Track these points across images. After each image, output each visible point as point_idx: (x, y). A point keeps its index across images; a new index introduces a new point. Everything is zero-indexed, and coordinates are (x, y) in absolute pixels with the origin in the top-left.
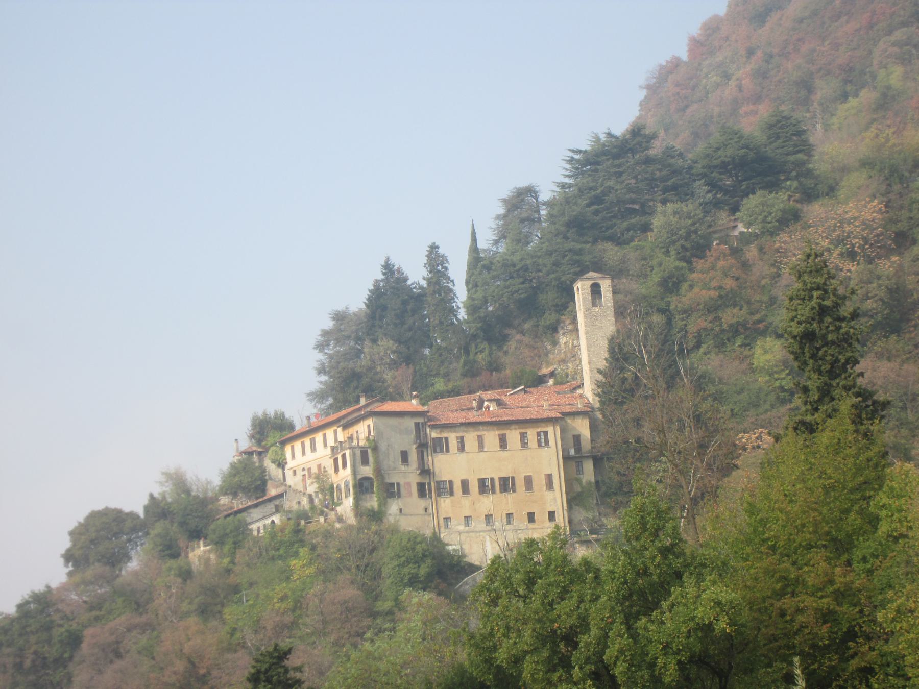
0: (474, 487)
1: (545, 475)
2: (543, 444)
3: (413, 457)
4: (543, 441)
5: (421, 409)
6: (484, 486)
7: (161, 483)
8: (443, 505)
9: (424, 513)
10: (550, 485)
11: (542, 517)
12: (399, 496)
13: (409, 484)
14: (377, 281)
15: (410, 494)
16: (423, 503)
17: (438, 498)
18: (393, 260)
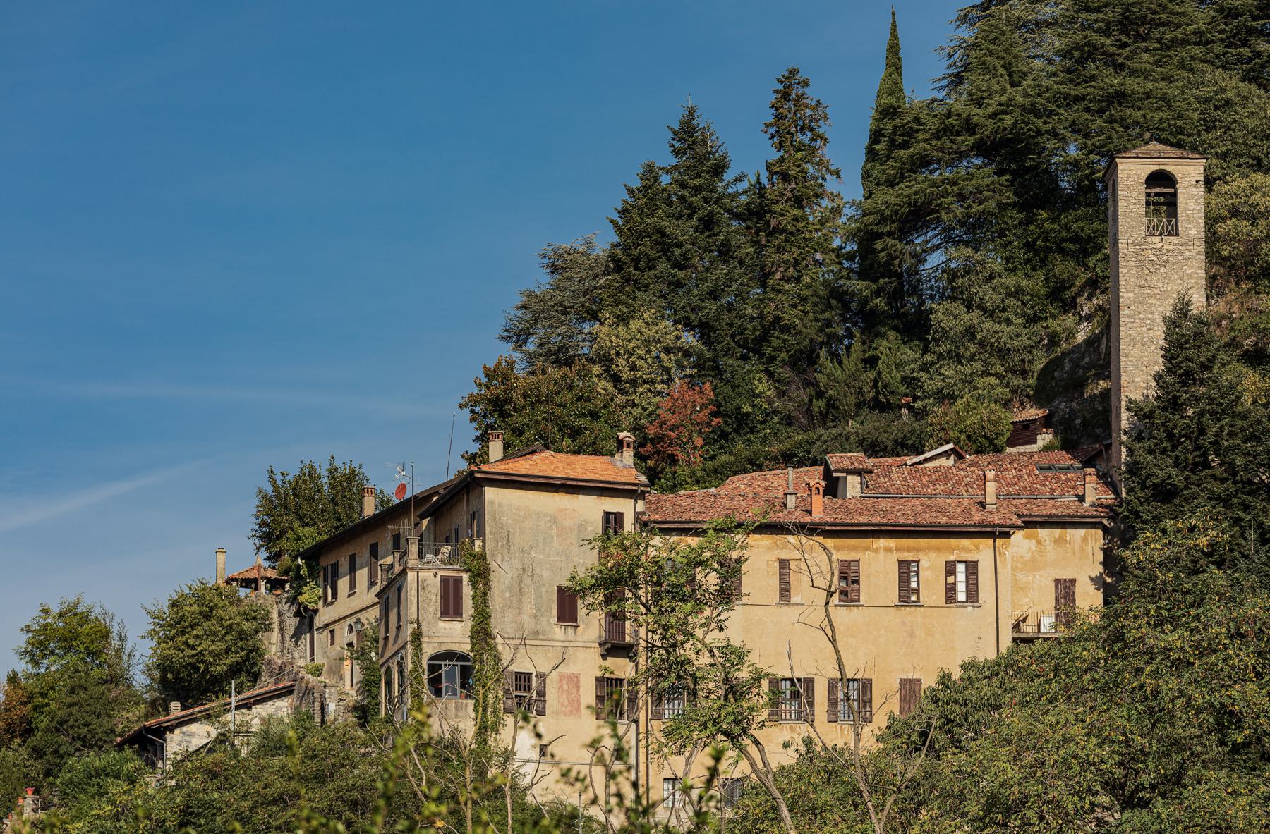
2: (962, 597)
4: (961, 587)
13: (574, 680)
18: (701, 121)
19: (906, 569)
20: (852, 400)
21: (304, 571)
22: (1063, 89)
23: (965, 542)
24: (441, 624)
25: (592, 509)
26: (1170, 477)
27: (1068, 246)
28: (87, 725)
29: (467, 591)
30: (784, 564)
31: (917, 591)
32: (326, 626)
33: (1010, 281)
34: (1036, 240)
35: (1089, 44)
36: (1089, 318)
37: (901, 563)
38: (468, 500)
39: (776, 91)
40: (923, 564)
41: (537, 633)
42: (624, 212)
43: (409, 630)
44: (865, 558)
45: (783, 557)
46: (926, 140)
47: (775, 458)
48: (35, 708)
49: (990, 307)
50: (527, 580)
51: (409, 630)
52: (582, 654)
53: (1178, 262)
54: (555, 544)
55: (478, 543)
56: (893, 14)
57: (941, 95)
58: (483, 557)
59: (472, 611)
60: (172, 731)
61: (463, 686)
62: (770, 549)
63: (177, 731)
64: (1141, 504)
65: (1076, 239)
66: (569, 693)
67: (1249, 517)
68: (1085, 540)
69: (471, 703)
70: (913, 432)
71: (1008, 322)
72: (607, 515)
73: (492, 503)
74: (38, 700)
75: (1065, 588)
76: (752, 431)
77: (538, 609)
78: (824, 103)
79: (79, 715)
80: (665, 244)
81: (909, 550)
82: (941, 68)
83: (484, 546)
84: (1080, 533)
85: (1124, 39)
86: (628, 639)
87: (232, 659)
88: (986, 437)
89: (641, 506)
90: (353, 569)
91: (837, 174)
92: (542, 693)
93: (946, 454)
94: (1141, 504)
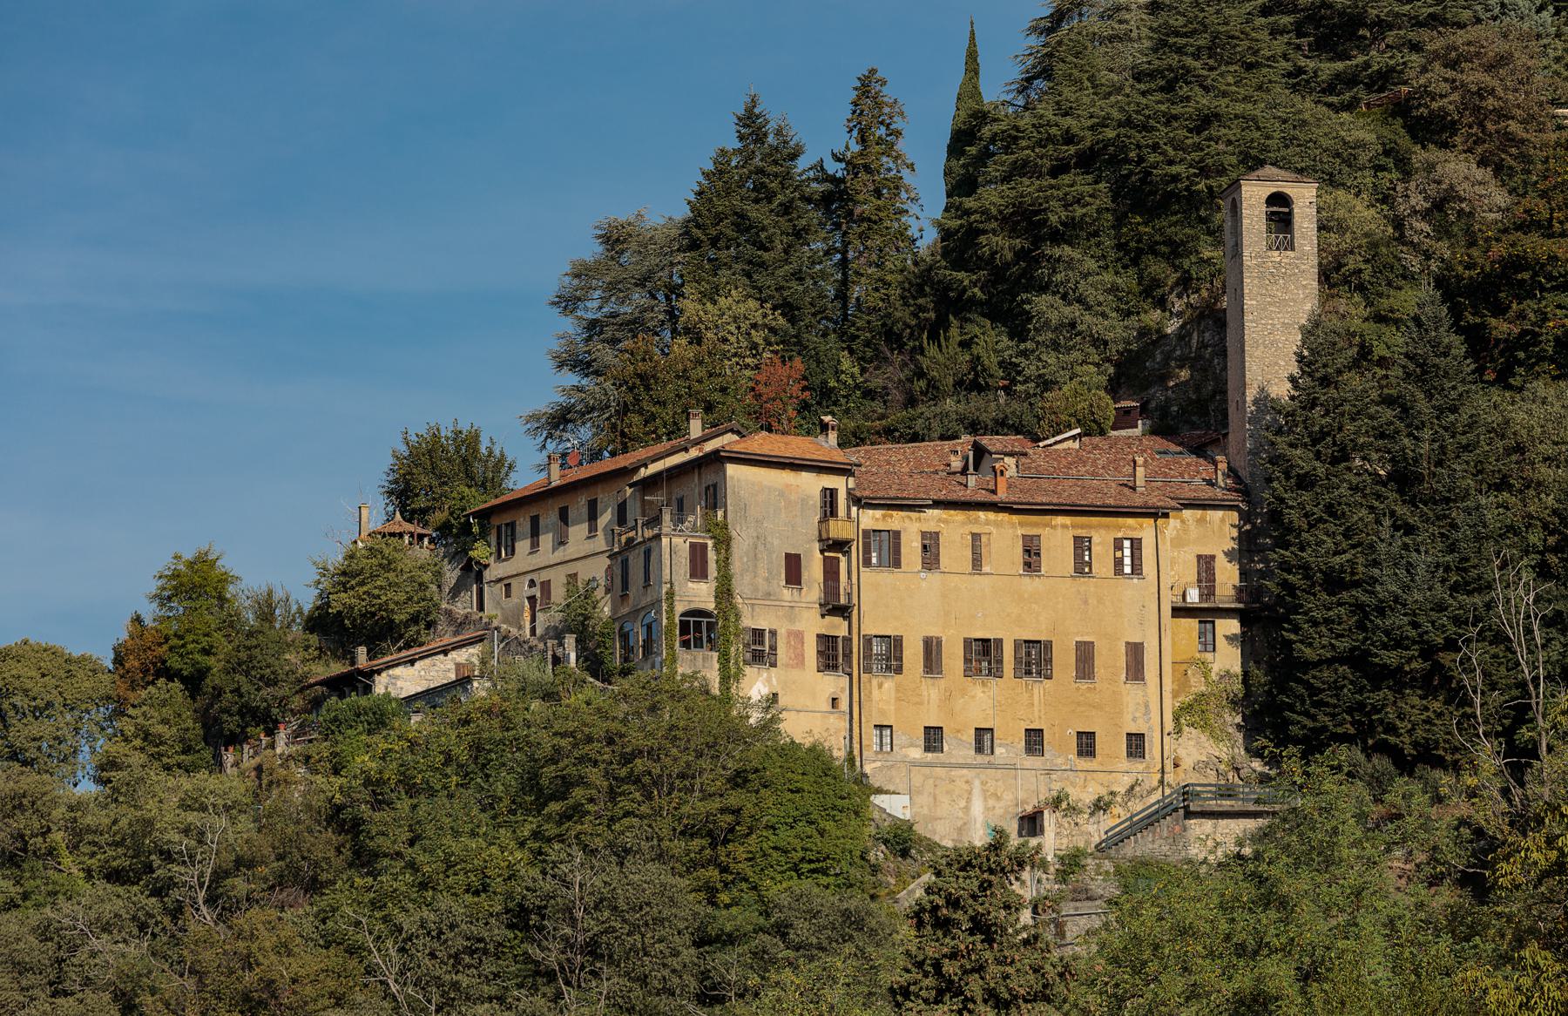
0: (953, 657)
1: (1128, 643)
2: (1127, 570)
3: (814, 569)
4: (1127, 561)
5: (839, 456)
6: (983, 654)
7: (206, 554)
8: (875, 693)
9: (829, 708)
10: (1135, 670)
11: (1111, 745)
12: (773, 665)
13: (799, 636)
14: (723, 152)
15: (800, 661)
16: (834, 684)
17: (864, 677)
18: (774, 113)
20: (951, 380)
21: (476, 529)
22: (1163, 108)
23: (1130, 521)
24: (690, 584)
25: (812, 485)
26: (1315, 469)
27: (1164, 249)
28: (268, 666)
29: (712, 555)
30: (976, 537)
31: (1090, 564)
32: (500, 580)
33: (1108, 277)
34: (1128, 242)
35: (1183, 67)
36: (1180, 314)
38: (700, 474)
39: (856, 89)
40: (1095, 540)
41: (770, 594)
42: (700, 193)
43: (665, 588)
44: (1045, 533)
45: (1206, 551)
46: (1027, 148)
47: (878, 433)
48: (171, 649)
49: (1091, 302)
50: (761, 548)
51: (665, 588)
52: (806, 614)
53: (1295, 274)
54: (783, 515)
55: (720, 513)
56: (972, 23)
58: (725, 526)
59: (716, 574)
60: (379, 674)
61: (710, 640)
62: (964, 523)
63: (384, 674)
64: (1286, 491)
65: (1169, 242)
66: (795, 648)
67: (1382, 506)
68: (1223, 520)
69: (715, 655)
70: (1013, 413)
71: (1104, 315)
73: (732, 478)
74: (174, 642)
75: (1206, 564)
76: (835, 403)
77: (770, 573)
78: (900, 101)
79: (260, 657)
80: (743, 223)
81: (1082, 527)
82: (1016, 73)
83: (725, 517)
84: (1219, 514)
85: (1211, 62)
86: (843, 601)
87: (412, 609)
88: (1094, 421)
89: (851, 482)
90: (535, 533)
91: (911, 167)
92: (773, 648)
93: (1074, 438)
94: (1286, 491)
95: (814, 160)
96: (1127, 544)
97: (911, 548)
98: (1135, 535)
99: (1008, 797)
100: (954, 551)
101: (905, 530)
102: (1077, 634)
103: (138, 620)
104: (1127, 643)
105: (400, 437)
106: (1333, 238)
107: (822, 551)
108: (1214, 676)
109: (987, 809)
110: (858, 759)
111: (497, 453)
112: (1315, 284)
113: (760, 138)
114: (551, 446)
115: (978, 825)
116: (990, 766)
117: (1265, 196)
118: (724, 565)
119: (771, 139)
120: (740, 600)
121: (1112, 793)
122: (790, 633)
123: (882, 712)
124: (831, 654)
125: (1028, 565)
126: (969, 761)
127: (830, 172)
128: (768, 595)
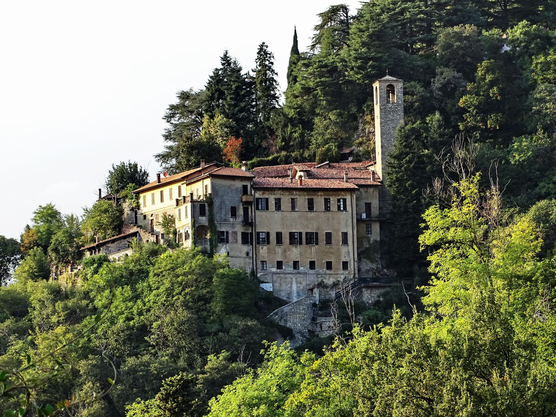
0: (286, 239)
2: (342, 209)
3: (241, 212)
4: (342, 206)
6: (295, 239)
8: (261, 251)
9: (246, 256)
12: (227, 242)
14: (216, 69)
16: (246, 248)
17: (257, 246)
18: (232, 55)
19: (327, 201)
24: (200, 218)
30: (293, 199)
31: (330, 207)
37: (325, 199)
40: (331, 199)
41: (226, 220)
44: (315, 197)
45: (292, 197)
52: (238, 226)
53: (396, 111)
57: (308, 51)
62: (289, 195)
72: (244, 186)
81: (327, 195)
82: (310, 43)
84: (372, 190)
91: (277, 74)
92: (227, 237)
95: (246, 72)
96: (342, 200)
97: (272, 203)
98: (345, 197)
99: (304, 283)
100: (286, 203)
101: (270, 198)
102: (326, 230)
103: (28, 227)
104: (342, 232)
105: (112, 166)
106: (409, 97)
107: (243, 205)
108: (371, 242)
109: (297, 287)
110: (255, 272)
111: (143, 170)
112: (403, 114)
113: (229, 64)
114: (164, 165)
115: (295, 292)
116: (299, 273)
117: (386, 86)
118: (211, 210)
119: (232, 65)
120: (216, 222)
121: (339, 281)
122: (233, 232)
123: (263, 257)
124: (246, 239)
125: (309, 208)
126: (291, 272)
127: (252, 76)
128: (225, 220)
